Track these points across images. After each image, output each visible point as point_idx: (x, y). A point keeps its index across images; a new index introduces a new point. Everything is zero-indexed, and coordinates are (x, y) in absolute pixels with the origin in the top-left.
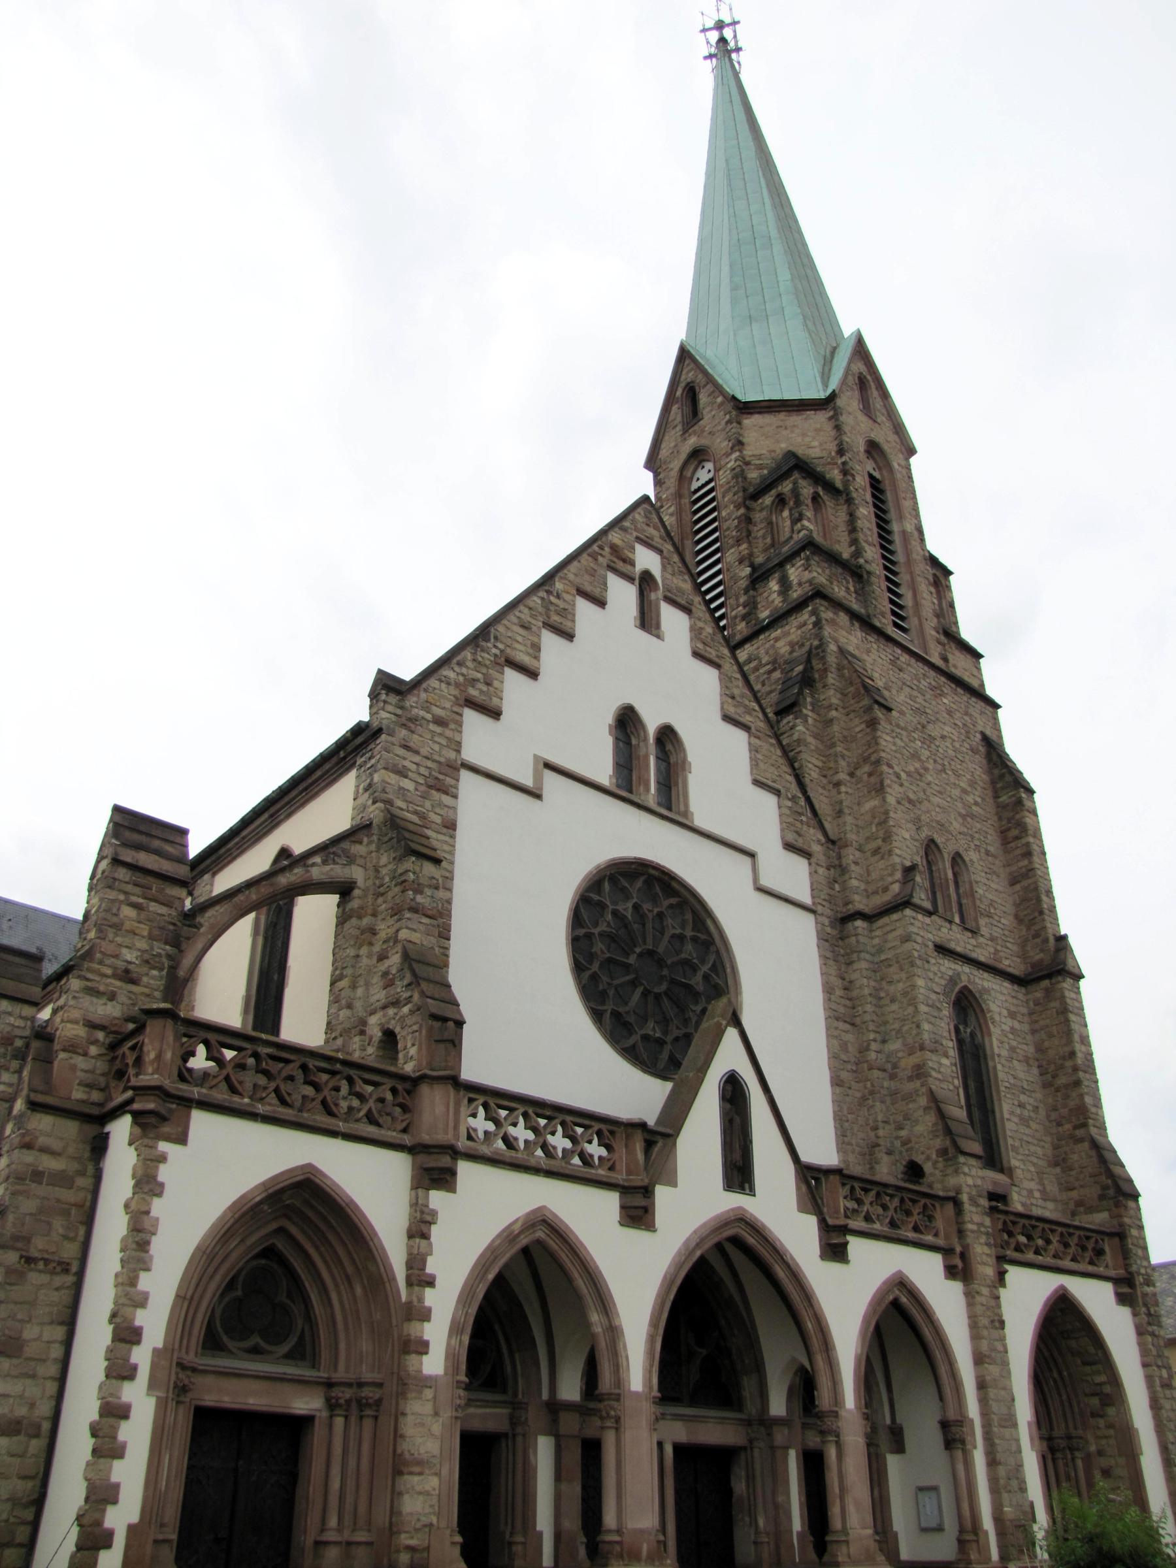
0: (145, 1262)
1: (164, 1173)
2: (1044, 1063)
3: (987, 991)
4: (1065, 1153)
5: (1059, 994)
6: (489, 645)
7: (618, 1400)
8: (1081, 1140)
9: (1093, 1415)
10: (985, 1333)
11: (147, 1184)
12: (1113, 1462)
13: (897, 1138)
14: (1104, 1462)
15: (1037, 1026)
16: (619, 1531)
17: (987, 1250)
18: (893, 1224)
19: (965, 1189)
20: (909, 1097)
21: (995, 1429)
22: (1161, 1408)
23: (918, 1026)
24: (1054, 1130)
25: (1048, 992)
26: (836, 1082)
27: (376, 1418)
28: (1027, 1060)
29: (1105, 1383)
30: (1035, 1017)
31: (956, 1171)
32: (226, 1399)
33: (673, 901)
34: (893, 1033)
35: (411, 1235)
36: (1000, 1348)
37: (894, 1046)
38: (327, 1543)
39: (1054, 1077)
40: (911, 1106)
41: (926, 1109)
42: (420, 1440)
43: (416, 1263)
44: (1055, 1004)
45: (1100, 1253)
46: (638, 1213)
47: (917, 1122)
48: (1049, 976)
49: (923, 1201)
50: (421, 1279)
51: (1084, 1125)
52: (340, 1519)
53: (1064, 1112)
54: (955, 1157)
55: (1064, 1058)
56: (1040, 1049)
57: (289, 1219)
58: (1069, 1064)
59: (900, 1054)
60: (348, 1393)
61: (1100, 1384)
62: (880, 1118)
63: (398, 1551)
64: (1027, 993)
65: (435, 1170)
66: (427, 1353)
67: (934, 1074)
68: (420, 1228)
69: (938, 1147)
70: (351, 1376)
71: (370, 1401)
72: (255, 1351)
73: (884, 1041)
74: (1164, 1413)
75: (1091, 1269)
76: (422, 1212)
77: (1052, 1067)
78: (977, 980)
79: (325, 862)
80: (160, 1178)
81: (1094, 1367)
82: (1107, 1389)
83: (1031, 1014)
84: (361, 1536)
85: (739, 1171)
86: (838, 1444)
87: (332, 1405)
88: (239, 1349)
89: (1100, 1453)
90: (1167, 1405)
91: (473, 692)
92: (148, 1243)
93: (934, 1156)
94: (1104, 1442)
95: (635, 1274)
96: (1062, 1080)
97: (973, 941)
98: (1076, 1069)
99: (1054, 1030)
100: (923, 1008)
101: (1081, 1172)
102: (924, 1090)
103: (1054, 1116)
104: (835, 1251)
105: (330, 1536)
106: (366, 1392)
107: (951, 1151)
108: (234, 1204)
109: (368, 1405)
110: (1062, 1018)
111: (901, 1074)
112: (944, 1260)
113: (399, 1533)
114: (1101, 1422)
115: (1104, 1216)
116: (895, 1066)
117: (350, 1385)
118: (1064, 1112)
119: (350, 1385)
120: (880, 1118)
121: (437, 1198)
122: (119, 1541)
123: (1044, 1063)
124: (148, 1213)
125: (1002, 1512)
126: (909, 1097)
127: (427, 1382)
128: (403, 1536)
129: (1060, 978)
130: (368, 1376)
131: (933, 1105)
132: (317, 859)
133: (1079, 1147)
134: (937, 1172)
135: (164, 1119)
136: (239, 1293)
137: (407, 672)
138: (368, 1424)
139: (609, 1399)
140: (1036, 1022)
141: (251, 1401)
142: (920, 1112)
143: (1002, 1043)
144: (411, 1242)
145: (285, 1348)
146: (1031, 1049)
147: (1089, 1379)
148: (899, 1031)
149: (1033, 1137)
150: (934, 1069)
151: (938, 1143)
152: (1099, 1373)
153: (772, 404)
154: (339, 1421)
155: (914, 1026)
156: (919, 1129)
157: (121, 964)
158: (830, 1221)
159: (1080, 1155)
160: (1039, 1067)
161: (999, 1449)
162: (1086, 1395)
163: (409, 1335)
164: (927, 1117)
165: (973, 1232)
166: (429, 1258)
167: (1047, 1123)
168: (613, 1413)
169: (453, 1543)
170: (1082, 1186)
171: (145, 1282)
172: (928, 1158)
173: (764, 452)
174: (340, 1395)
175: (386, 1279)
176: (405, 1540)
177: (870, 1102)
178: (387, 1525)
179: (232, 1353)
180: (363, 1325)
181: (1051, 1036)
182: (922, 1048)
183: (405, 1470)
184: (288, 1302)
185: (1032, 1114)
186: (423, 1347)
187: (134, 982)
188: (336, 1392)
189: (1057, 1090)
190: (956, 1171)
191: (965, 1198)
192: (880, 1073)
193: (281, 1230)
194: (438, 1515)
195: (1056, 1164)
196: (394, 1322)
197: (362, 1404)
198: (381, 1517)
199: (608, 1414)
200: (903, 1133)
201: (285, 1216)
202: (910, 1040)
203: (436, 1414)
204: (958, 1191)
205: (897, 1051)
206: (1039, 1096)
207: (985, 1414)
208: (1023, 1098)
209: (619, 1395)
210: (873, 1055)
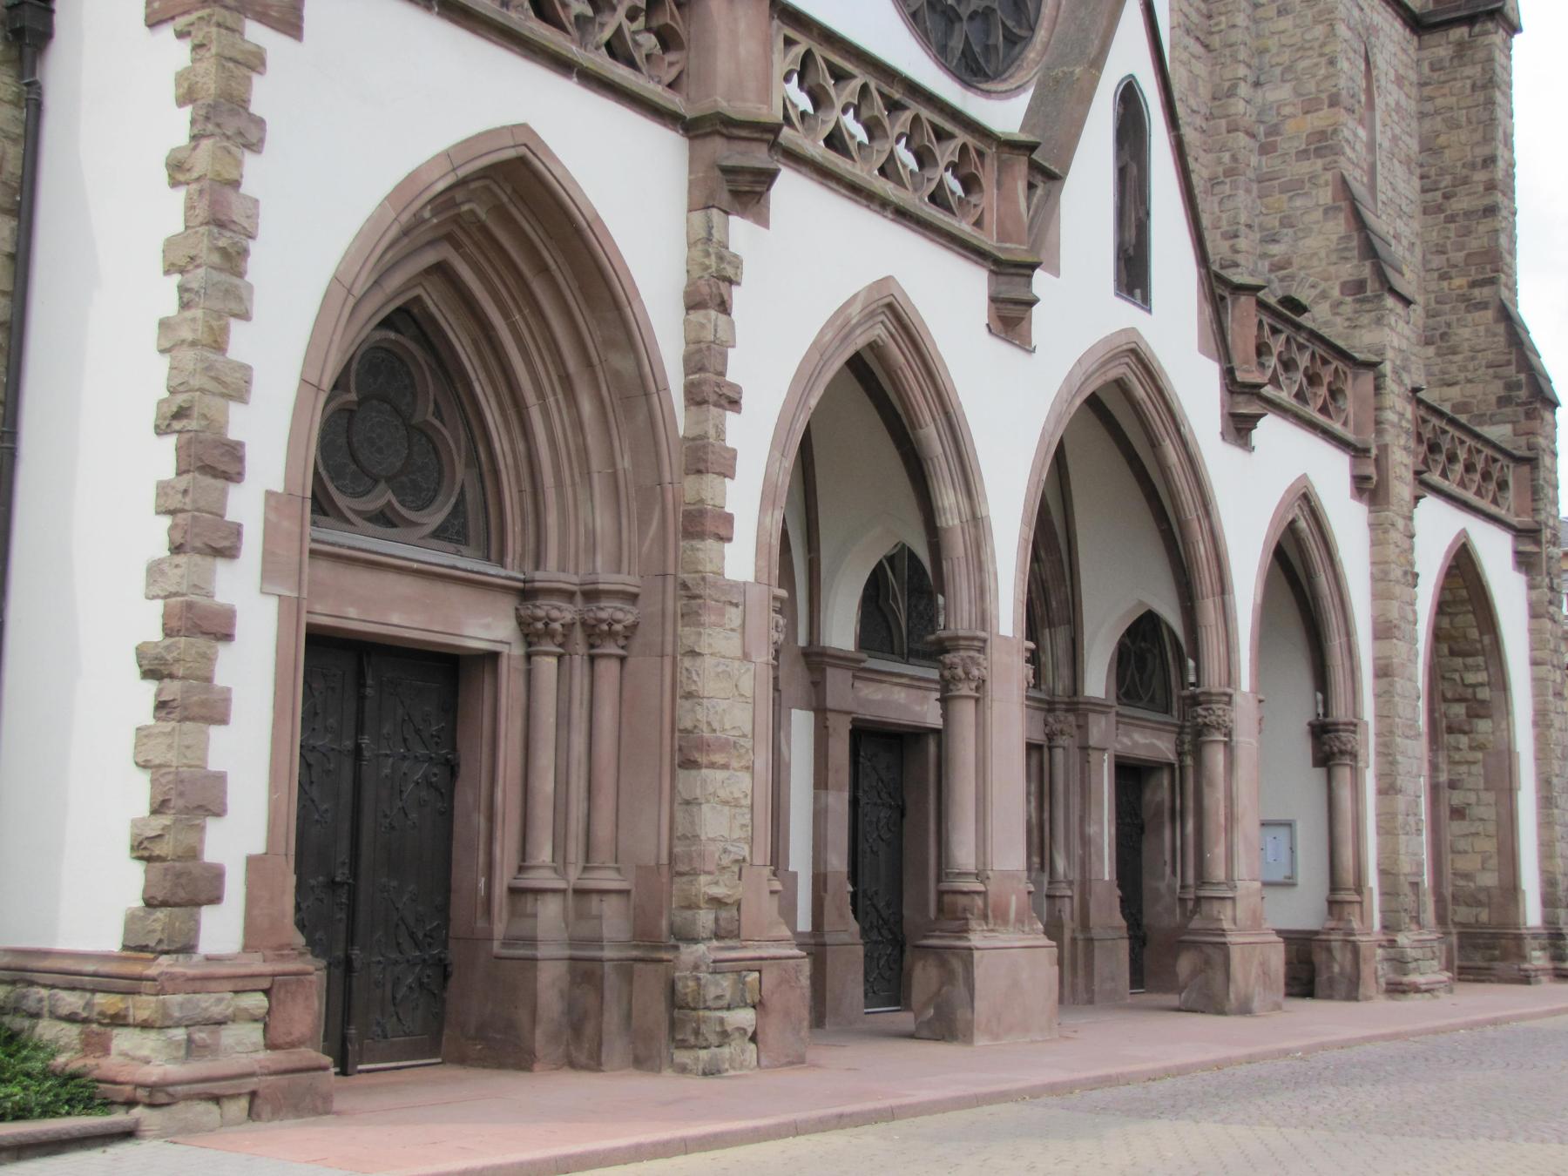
0: (240, 299)
1: (263, 96)
2: (1433, 172)
4: (1449, 325)
5: (1481, 55)
7: (981, 650)
8: (1483, 306)
9: (1450, 730)
10: (1398, 590)
11: (224, 116)
12: (1472, 798)
13: (1264, 256)
14: (1457, 798)
15: (1429, 107)
16: (980, 876)
17: (1408, 460)
18: (1300, 396)
19: (1390, 354)
20: (1294, 188)
21: (1399, 740)
22: (1550, 726)
23: (1332, 62)
24: (1433, 286)
25: (1461, 47)
27: (622, 659)
28: (1407, 162)
29: (1482, 685)
30: (1427, 91)
31: (1379, 321)
32: (352, 612)
34: (1278, 71)
35: (694, 303)
36: (1411, 618)
37: (1279, 93)
38: (538, 892)
39: (1446, 197)
40: (1298, 203)
41: (1328, 211)
42: (724, 704)
43: (705, 361)
44: (1473, 71)
45: (1502, 485)
46: (1011, 318)
47: (1308, 231)
48: (1470, 20)
49: (1335, 363)
50: (712, 391)
51: (1492, 281)
52: (559, 846)
53: (1458, 257)
54: (1379, 297)
55: (1473, 166)
56: (1429, 147)
57: (457, 246)
58: (1480, 176)
59: (1287, 111)
60: (566, 612)
61: (1474, 686)
62: (1243, 219)
63: (691, 906)
64: (1420, 48)
65: (736, 182)
66: (729, 540)
67: (1348, 151)
68: (710, 291)
69: (1346, 278)
70: (570, 580)
71: (618, 627)
72: (384, 519)
73: (1257, 84)
74: (1554, 734)
76: (721, 258)
77: (1447, 180)
80: (255, 108)
81: (1470, 661)
82: (1484, 694)
83: (1422, 85)
84: (606, 879)
85: (1133, 274)
86: (1229, 747)
87: (531, 633)
88: (358, 513)
89: (1453, 785)
90: (1558, 722)
92: (244, 253)
93: (1336, 293)
94: (1463, 769)
96: (1460, 204)
98: (1491, 186)
99: (1462, 116)
100: (1342, 30)
101: (1473, 359)
102: (1329, 176)
103: (1437, 261)
104: (1239, 428)
105: (542, 878)
106: (608, 610)
107: (1372, 287)
108: (399, 188)
109: (611, 634)
110: (1480, 96)
111: (1283, 145)
112: (1353, 466)
113: (694, 873)
114: (1464, 741)
115: (1507, 429)
116: (1274, 130)
117: (569, 595)
118: (1458, 257)
119: (569, 595)
120: (1243, 219)
123: (1433, 172)
124: (235, 184)
125: (1396, 862)
126: (1294, 188)
127: (734, 595)
128: (703, 879)
129: (1490, 26)
130: (608, 579)
131: (1344, 204)
133: (1476, 315)
134: (1338, 320)
136: (353, 396)
138: (608, 671)
139: (968, 648)
140: (1431, 99)
141: (395, 619)
142: (1318, 215)
143: (1385, 125)
144: (697, 316)
145: (435, 518)
146: (1414, 145)
147: (1456, 676)
148: (1289, 69)
150: (1347, 141)
151: (1350, 269)
152: (1477, 668)
154: (547, 666)
155: (1323, 60)
156: (1311, 243)
158: (1240, 376)
159: (1474, 330)
160: (1422, 177)
161: (1401, 769)
162: (1445, 700)
163: (701, 501)
164: (1330, 225)
165: (1393, 425)
166: (731, 352)
167: (1422, 274)
168: (975, 672)
169: (772, 892)
170: (1469, 381)
171: (242, 343)
172: (1324, 295)
174: (555, 614)
175: (653, 388)
176: (706, 886)
177: (1227, 189)
178: (664, 859)
179: (348, 521)
180: (596, 477)
181: (1454, 125)
182: (1334, 102)
183: (702, 759)
184: (437, 423)
185: (1407, 254)
188: (544, 608)
189: (1451, 219)
190: (1379, 321)
191: (1387, 368)
192: (1247, 139)
193: (442, 270)
194: (752, 841)
195: (1428, 342)
196: (667, 477)
197: (594, 633)
198: (648, 845)
199: (967, 674)
200: (1275, 249)
201: (449, 238)
202: (1311, 87)
203: (746, 656)
204: (1380, 352)
205: (1280, 105)
206: (1416, 225)
207: (1380, 717)
209: (985, 641)
210: (1241, 106)
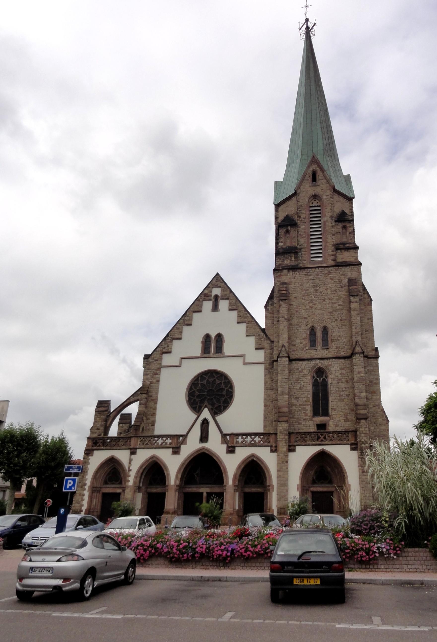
3: (331, 365)
26: (265, 406)
33: (219, 375)
50: (130, 470)
65: (133, 452)
75: (331, 443)
91: (164, 350)
97: (327, 352)
121: (133, 456)
122: (84, 511)
135: (89, 453)
149: (345, 404)
157: (97, 427)
186: (129, 481)
187: (99, 429)
208: (341, 393)
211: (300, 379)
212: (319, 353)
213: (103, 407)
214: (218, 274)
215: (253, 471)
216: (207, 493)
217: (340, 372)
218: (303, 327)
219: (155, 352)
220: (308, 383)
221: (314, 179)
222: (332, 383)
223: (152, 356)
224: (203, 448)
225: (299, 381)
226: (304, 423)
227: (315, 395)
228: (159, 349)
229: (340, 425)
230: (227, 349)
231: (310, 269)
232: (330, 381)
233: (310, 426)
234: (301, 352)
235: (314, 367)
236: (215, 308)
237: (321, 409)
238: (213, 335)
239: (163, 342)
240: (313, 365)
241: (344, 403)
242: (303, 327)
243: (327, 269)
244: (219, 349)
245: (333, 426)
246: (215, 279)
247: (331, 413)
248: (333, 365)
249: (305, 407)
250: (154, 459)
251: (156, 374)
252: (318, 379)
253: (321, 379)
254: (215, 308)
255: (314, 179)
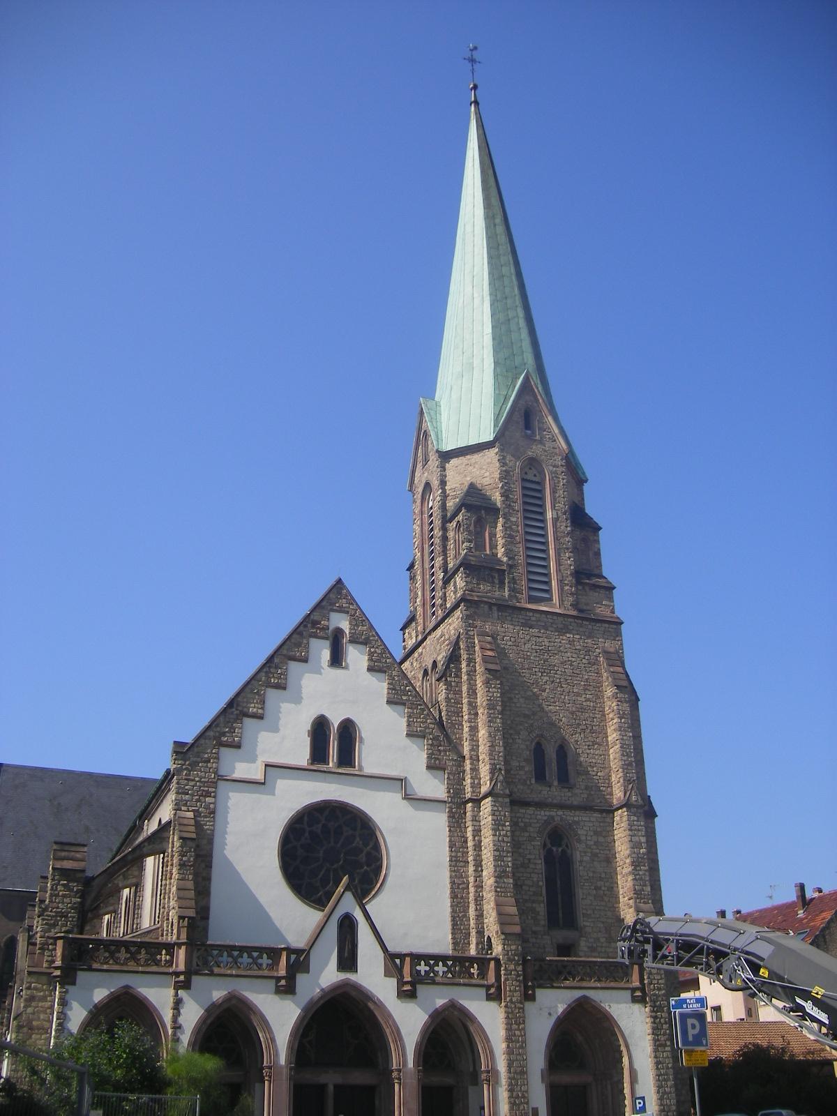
3: (577, 823)
6: (234, 710)
50: (177, 1027)
78: (568, 818)
79: (149, 845)
95: (280, 1017)
97: (570, 794)
132: (146, 844)
137: (189, 738)
153: (461, 450)
173: (458, 485)
208: (599, 884)
211: (523, 847)
212: (555, 793)
213: (72, 859)
214: (339, 581)
215: (449, 1040)
216: (336, 1086)
217: (595, 838)
218: (524, 734)
219: (202, 741)
220: (537, 857)
221: (528, 425)
222: (581, 862)
223: (196, 750)
224: (346, 984)
225: (521, 851)
226: (534, 940)
227: (550, 881)
228: (211, 733)
229: (599, 949)
230: (370, 758)
231: (531, 614)
232: (577, 856)
233: (544, 948)
234: (522, 787)
235: (547, 823)
236: (337, 659)
237: (560, 912)
238: (335, 722)
239: (221, 719)
240: (545, 818)
241: (604, 903)
242: (524, 734)
243: (561, 619)
244: (347, 758)
245: (585, 949)
246: (334, 590)
247: (582, 922)
248: (582, 824)
249: (534, 905)
250: (234, 1002)
251: (208, 794)
252: (554, 849)
253: (560, 850)
254: (337, 659)
255: (528, 425)
